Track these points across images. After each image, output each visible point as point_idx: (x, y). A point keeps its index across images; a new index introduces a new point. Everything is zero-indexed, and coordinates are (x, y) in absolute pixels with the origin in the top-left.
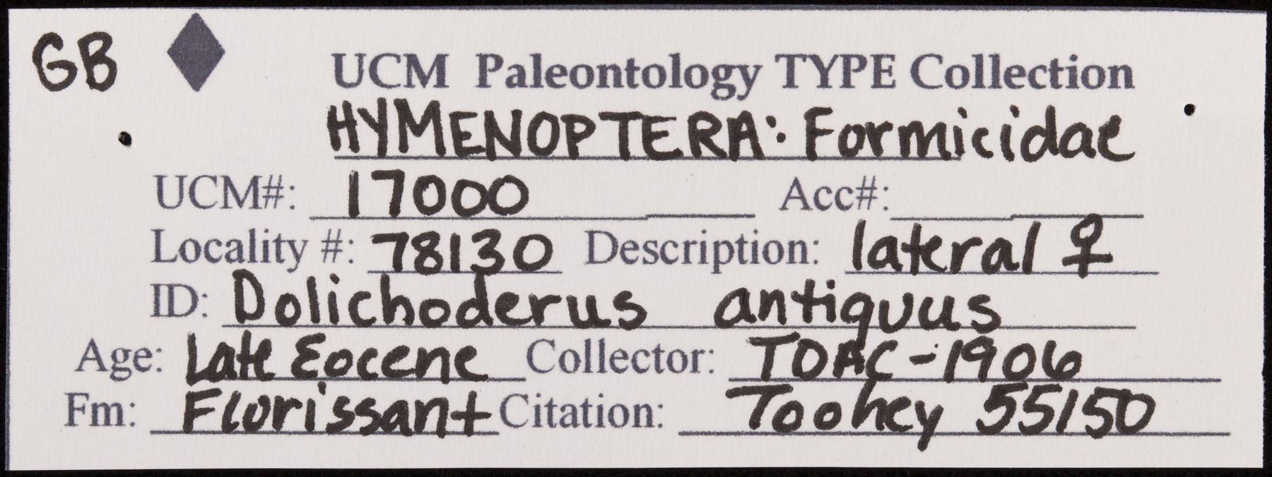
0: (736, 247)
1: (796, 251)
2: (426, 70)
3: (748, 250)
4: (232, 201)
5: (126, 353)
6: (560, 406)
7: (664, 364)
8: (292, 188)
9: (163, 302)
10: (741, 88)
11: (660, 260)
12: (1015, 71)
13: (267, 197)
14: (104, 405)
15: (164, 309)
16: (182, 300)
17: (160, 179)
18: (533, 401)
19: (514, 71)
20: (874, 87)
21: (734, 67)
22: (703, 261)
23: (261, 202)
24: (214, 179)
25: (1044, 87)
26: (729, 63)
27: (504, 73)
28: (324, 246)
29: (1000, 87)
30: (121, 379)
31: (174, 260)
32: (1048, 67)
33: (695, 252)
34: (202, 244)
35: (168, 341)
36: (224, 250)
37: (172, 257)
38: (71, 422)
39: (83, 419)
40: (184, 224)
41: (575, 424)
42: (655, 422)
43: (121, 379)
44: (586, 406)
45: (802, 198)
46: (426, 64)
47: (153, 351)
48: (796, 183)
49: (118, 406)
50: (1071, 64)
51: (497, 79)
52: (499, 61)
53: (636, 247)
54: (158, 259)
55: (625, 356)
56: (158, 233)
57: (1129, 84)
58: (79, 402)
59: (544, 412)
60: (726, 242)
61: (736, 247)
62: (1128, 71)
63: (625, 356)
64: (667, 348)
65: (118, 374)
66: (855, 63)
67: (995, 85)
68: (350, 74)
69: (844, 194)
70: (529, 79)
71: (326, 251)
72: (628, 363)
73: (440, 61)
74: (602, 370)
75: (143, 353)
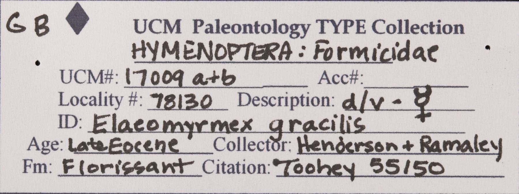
1: (325, 101)
2: (172, 26)
4: (92, 80)
5: (48, 142)
6: (227, 164)
7: (270, 148)
8: (362, 75)
9: (63, 122)
10: (302, 34)
11: (269, 105)
13: (106, 79)
14: (39, 164)
15: (64, 125)
16: (71, 121)
17: (62, 71)
18: (216, 163)
20: (357, 33)
21: (299, 25)
22: (286, 105)
23: (104, 81)
24: (85, 71)
25: (427, 33)
26: (297, 23)
27: (204, 27)
28: (130, 99)
29: (458, 33)
31: (68, 105)
32: (429, 24)
33: (283, 101)
34: (80, 99)
36: (88, 101)
38: (25, 172)
39: (30, 170)
40: (72, 90)
41: (233, 172)
42: (267, 171)
44: (238, 165)
45: (327, 79)
46: (172, 23)
47: (59, 142)
48: (325, 73)
50: (438, 24)
51: (201, 30)
52: (202, 22)
53: (259, 99)
54: (61, 104)
55: (254, 144)
56: (61, 93)
57: (462, 32)
58: (28, 163)
60: (296, 98)
61: (300, 99)
62: (462, 26)
63: (254, 144)
65: (44, 152)
66: (349, 23)
68: (141, 28)
69: (345, 77)
70: (215, 30)
71: (131, 101)
72: (256, 147)
73: (178, 22)
74: (245, 150)
75: (55, 143)
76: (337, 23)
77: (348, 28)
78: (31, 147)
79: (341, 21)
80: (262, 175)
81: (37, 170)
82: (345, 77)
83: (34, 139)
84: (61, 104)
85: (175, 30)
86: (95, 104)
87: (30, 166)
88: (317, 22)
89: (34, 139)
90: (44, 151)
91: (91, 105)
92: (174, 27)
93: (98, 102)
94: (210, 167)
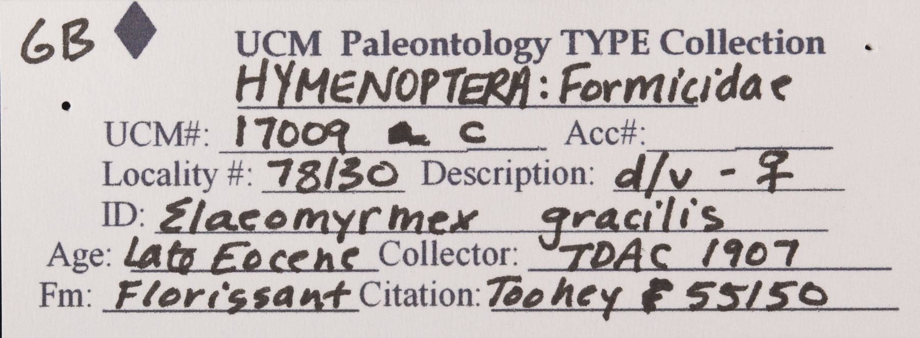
0: (533, 172)
1: (577, 175)
3: (542, 174)
4: (162, 140)
5: (84, 252)
7: (480, 259)
9: (111, 215)
10: (536, 55)
12: (737, 42)
14: (69, 291)
15: (112, 220)
16: (126, 214)
17: (109, 124)
18: (384, 286)
19: (369, 43)
21: (530, 39)
22: (509, 182)
23: (184, 141)
24: (149, 124)
25: (756, 53)
27: (362, 45)
30: (81, 272)
33: (503, 175)
35: (117, 242)
36: (156, 176)
37: (118, 182)
38: (44, 304)
39: (53, 302)
40: (127, 158)
41: (415, 304)
42: (474, 301)
43: (81, 272)
46: (305, 38)
47: (104, 251)
48: (577, 125)
49: (78, 291)
50: (778, 36)
51: (357, 49)
52: (358, 36)
53: (459, 173)
55: (452, 253)
56: (107, 164)
57: (821, 50)
58: (50, 288)
59: (392, 295)
60: (526, 169)
61: (533, 172)
62: (820, 40)
63: (452, 253)
64: (483, 247)
65: (78, 268)
66: (619, 36)
67: (723, 51)
69: (612, 132)
71: (231, 177)
72: (454, 257)
73: (315, 35)
74: (435, 263)
75: (96, 253)
76: (598, 36)
77: (618, 45)
78: (55, 260)
79: (605, 32)
80: (465, 309)
81: (66, 301)
82: (612, 132)
83: (59, 246)
84: (107, 184)
85: (310, 50)
86: (168, 183)
87: (52, 294)
88: (562, 34)
89: (59, 246)
90: (78, 268)
91: (160, 184)
92: (309, 43)
93: (172, 180)
94: (374, 294)
